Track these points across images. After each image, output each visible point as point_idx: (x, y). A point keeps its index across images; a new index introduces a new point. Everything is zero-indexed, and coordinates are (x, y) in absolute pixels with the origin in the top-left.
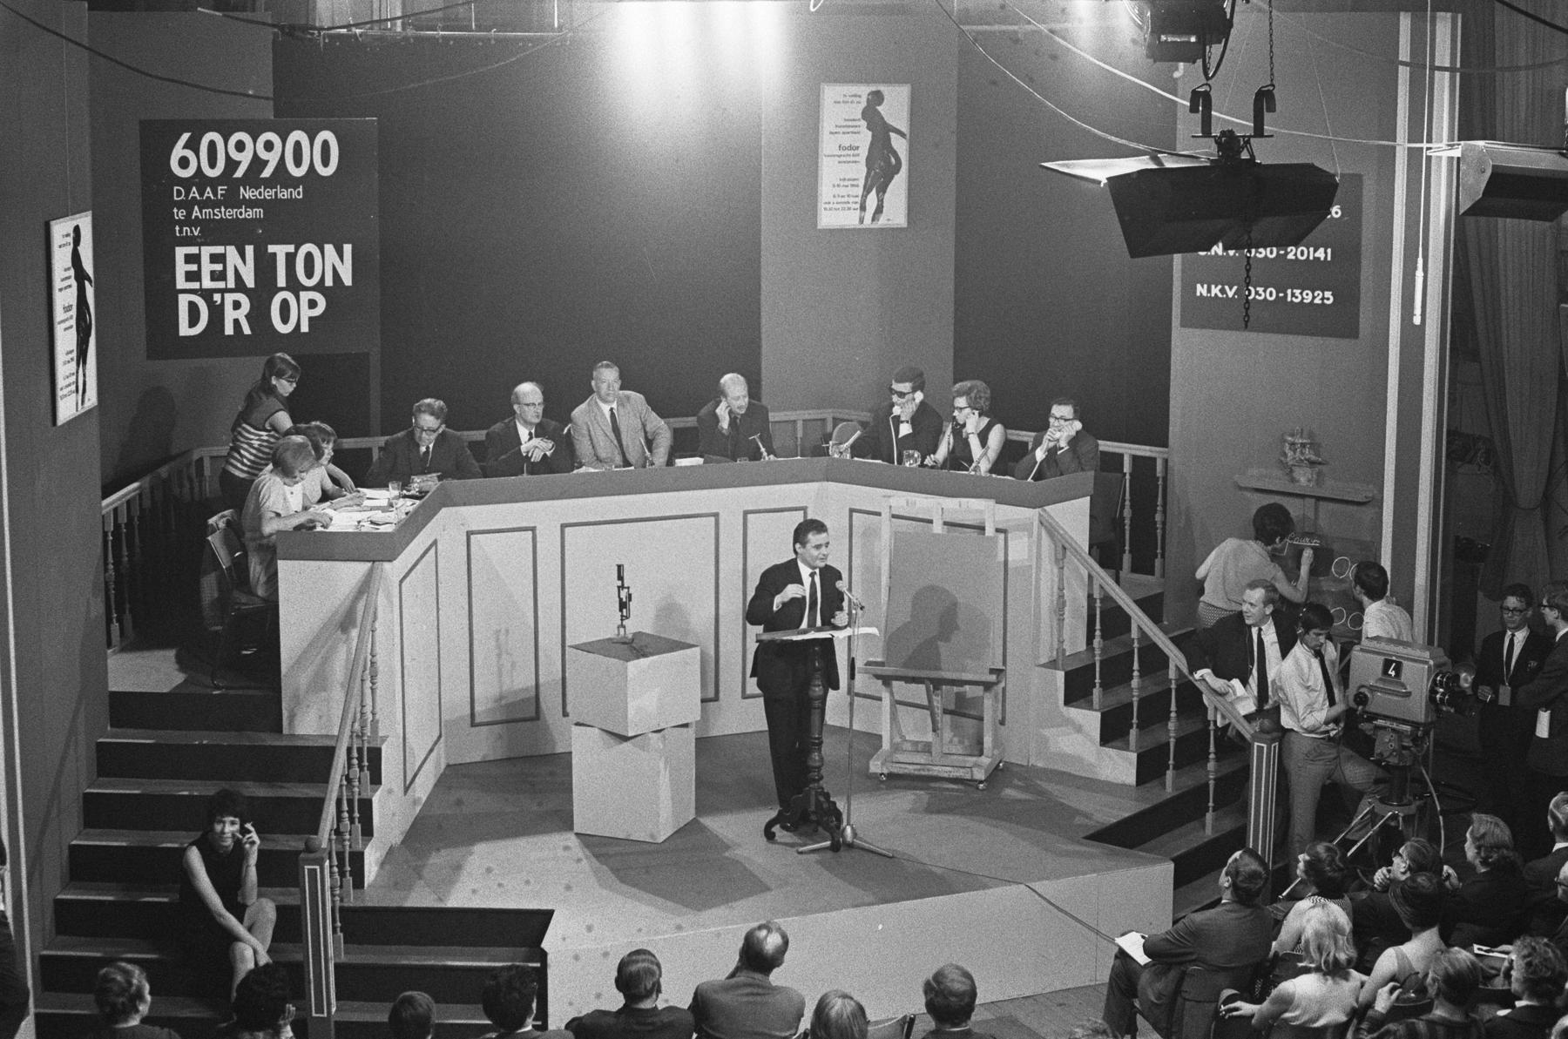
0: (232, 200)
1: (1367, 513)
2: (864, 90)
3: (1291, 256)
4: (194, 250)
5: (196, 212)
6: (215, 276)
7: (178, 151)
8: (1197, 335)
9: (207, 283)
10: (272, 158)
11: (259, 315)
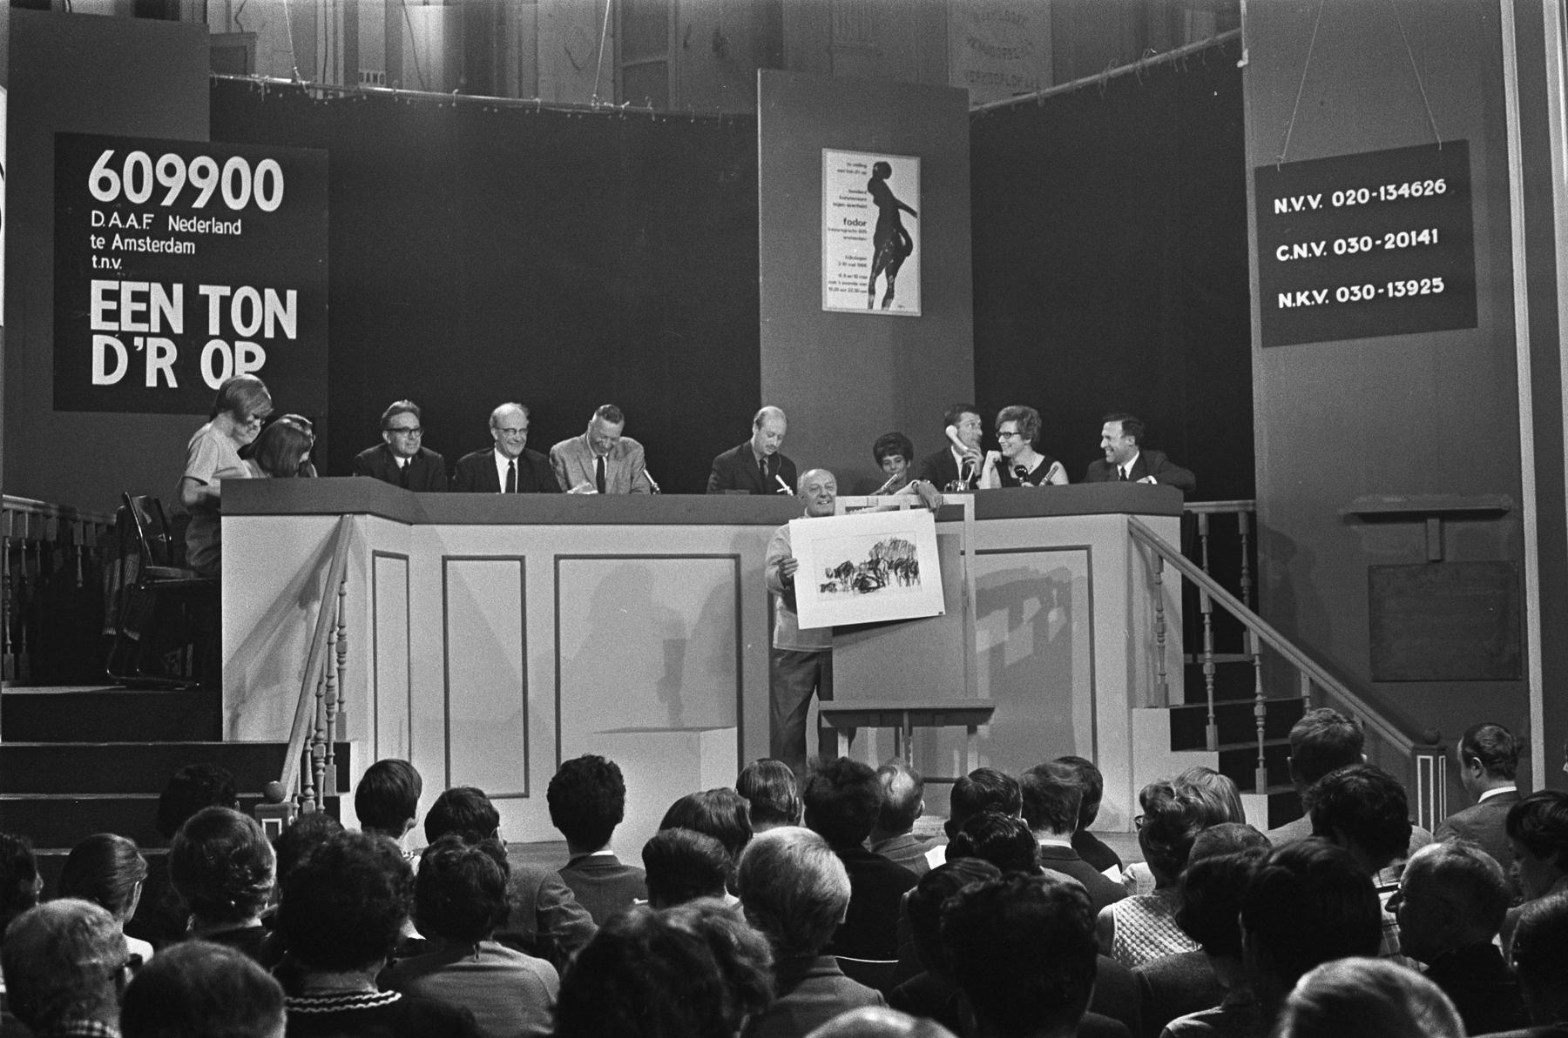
0: (159, 230)
1: (1505, 525)
2: (870, 160)
3: (1389, 246)
4: (112, 285)
5: (117, 242)
7: (98, 171)
9: (127, 325)
11: (187, 365)
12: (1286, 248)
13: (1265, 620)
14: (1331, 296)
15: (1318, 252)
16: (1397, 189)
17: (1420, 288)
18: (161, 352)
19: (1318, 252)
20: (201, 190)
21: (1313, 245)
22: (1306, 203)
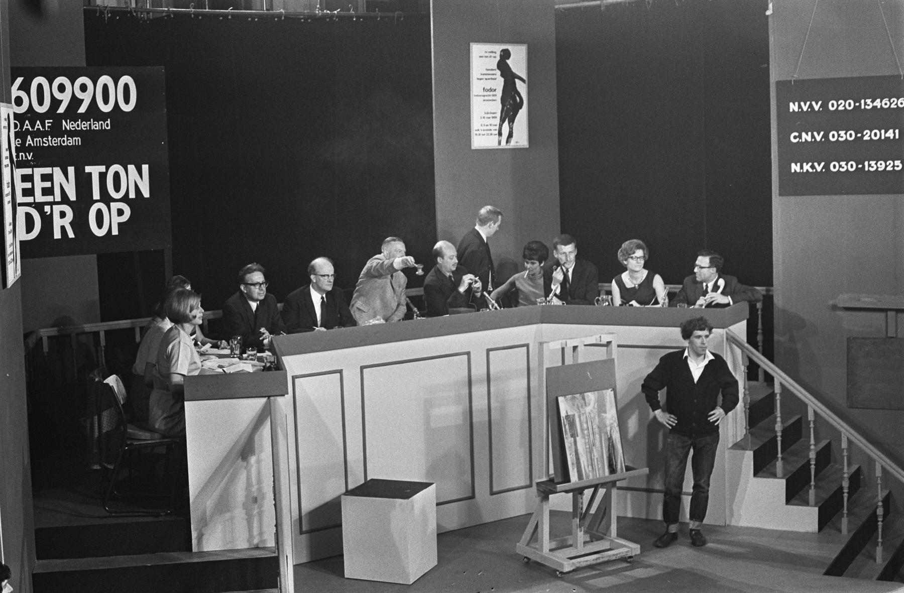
0: (57, 131)
2: (498, 48)
3: (866, 138)
4: (28, 171)
6: (47, 192)
8: (793, 200)
9: (39, 198)
10: (87, 98)
11: (80, 223)
12: (797, 134)
13: (778, 367)
14: (826, 167)
15: (818, 138)
16: (873, 102)
17: (886, 166)
18: (63, 215)
19: (818, 138)
20: (83, 100)
21: (815, 134)
22: (811, 106)
